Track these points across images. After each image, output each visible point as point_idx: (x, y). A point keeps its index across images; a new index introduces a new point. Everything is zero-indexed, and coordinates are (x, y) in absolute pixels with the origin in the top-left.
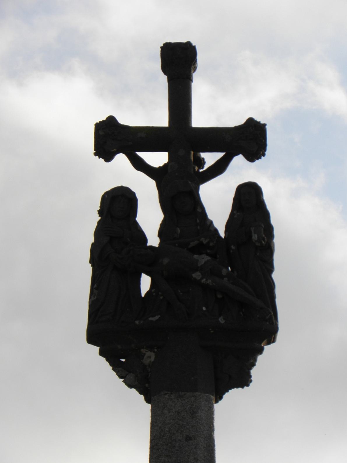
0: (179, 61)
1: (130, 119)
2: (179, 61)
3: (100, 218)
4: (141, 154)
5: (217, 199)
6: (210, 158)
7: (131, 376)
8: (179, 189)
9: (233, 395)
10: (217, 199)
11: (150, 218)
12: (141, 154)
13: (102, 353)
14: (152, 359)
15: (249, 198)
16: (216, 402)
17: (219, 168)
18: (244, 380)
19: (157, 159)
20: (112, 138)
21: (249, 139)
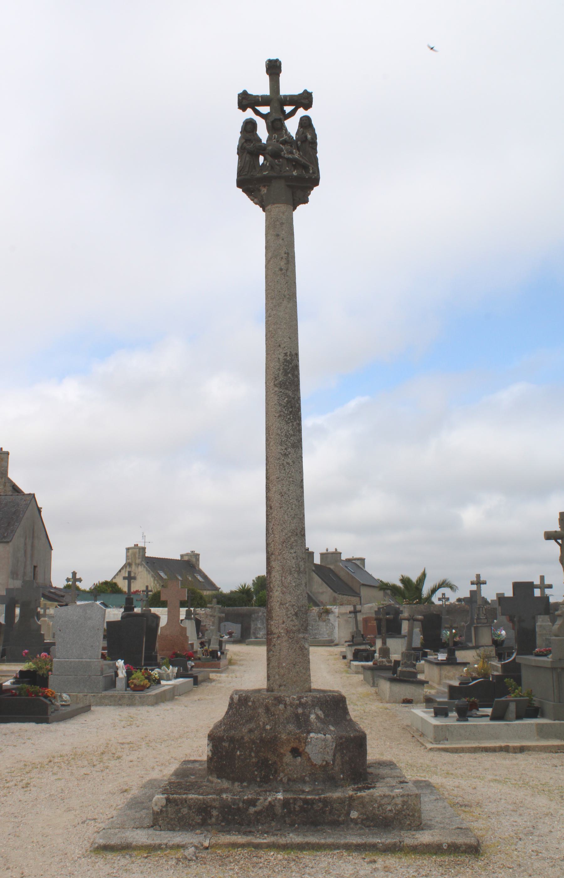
0: (274, 68)
1: (253, 91)
2: (274, 68)
3: (482, 596)
4: (258, 108)
5: (292, 126)
6: (288, 109)
7: (256, 200)
8: (276, 125)
9: (301, 208)
10: (292, 126)
11: (263, 133)
12: (258, 108)
13: (243, 191)
14: (265, 192)
15: (306, 123)
16: (294, 210)
17: (292, 113)
18: (306, 201)
19: (265, 110)
20: (246, 101)
21: (305, 100)
